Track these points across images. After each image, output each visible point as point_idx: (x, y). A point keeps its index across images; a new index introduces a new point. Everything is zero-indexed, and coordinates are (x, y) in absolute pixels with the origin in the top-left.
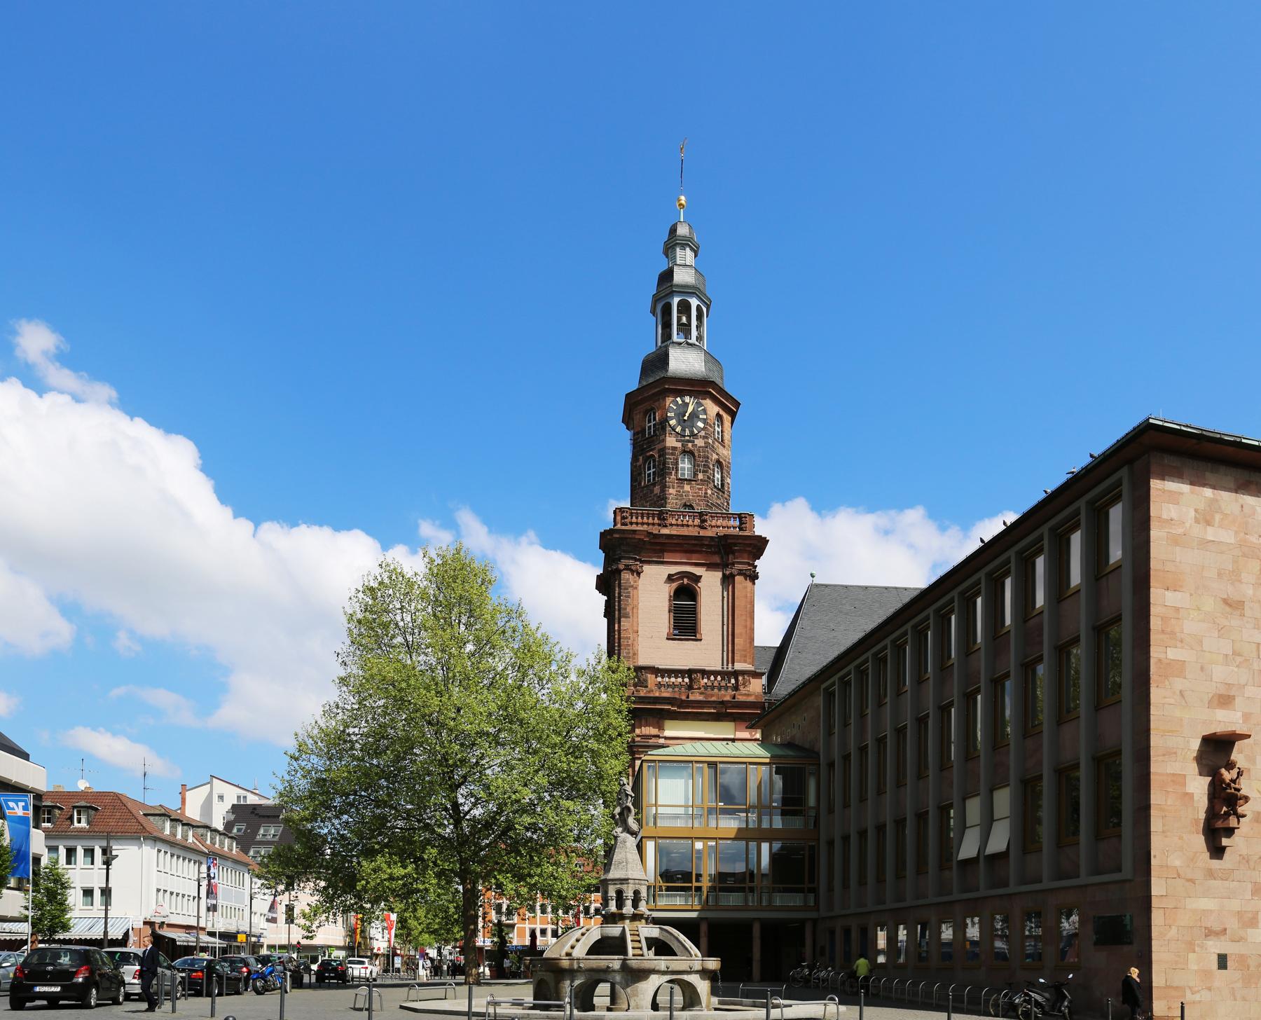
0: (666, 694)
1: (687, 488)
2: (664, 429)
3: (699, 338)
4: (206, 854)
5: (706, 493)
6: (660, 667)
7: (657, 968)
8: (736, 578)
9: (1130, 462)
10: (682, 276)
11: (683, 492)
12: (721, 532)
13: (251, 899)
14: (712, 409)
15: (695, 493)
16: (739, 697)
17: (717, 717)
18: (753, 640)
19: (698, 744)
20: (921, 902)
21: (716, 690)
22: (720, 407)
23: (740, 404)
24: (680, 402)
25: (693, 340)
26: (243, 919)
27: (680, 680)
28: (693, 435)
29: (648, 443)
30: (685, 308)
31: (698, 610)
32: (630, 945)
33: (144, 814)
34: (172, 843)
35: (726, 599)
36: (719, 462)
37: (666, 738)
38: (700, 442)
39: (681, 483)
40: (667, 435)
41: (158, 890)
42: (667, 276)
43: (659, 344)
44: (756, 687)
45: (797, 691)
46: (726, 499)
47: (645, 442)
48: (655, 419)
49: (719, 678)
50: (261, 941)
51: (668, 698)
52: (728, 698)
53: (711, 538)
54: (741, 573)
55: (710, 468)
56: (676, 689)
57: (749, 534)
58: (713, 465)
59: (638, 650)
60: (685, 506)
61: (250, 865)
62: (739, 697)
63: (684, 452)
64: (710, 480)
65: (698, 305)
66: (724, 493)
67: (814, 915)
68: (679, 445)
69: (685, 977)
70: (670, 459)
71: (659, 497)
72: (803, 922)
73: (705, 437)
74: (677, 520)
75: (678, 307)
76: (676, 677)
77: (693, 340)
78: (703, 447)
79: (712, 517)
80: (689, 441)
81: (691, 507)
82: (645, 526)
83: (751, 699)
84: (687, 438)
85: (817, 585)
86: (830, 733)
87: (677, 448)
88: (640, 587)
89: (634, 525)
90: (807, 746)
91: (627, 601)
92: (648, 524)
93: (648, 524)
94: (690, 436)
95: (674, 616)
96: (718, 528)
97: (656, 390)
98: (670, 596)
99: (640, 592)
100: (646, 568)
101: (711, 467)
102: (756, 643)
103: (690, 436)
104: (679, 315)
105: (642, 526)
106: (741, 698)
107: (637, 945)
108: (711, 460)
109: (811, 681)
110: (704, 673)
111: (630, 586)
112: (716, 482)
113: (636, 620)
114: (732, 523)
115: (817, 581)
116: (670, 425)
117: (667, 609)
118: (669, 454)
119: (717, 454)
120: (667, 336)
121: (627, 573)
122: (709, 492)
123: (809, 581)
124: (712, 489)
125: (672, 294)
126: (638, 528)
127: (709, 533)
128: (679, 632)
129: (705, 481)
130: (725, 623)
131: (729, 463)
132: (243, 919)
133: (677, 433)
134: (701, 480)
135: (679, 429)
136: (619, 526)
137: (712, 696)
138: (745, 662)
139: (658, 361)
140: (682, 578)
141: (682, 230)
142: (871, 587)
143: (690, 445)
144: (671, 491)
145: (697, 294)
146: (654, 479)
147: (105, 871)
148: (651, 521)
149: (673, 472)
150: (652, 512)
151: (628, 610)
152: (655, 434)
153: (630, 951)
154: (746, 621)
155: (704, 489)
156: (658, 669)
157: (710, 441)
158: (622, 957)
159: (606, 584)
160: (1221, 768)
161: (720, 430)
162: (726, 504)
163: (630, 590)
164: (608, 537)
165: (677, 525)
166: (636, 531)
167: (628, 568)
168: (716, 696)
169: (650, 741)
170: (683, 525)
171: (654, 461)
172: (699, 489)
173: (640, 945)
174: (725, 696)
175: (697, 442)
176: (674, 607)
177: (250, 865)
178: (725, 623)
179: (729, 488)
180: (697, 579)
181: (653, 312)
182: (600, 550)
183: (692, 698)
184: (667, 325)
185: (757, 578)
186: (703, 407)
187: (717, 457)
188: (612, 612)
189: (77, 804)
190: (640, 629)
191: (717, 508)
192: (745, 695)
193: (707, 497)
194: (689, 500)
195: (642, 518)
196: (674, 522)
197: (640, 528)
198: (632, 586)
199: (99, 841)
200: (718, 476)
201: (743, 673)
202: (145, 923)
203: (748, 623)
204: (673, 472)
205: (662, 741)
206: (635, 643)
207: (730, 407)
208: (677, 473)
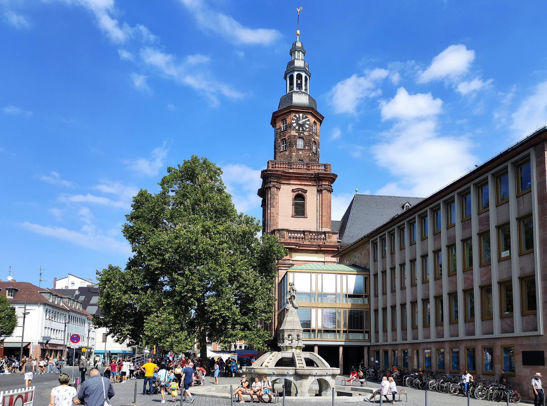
0: (293, 241)
1: (300, 153)
2: (290, 127)
3: (306, 90)
4: (68, 310)
5: (309, 155)
6: (290, 229)
7: (311, 374)
8: (323, 191)
9: (534, 146)
10: (299, 63)
12: (317, 172)
13: (89, 332)
14: (312, 119)
17: (316, 252)
19: (311, 264)
20: (428, 340)
21: (316, 240)
22: (315, 119)
23: (324, 118)
24: (298, 116)
25: (303, 90)
26: (83, 341)
27: (299, 235)
29: (283, 133)
30: (299, 77)
32: (297, 362)
33: (40, 293)
34: (53, 306)
35: (318, 200)
36: (314, 142)
37: (293, 261)
40: (292, 130)
41: (46, 328)
42: (292, 63)
44: (334, 239)
45: (358, 242)
46: (318, 157)
47: (282, 133)
48: (286, 123)
49: (314, 235)
50: (91, 351)
51: (295, 243)
52: (321, 244)
53: (312, 174)
54: (325, 189)
56: (298, 239)
57: (329, 173)
58: (312, 143)
61: (88, 316)
63: (300, 138)
64: (311, 149)
65: (305, 76)
66: (317, 155)
67: (369, 344)
68: (297, 134)
69: (323, 378)
72: (362, 347)
77: (303, 90)
79: (312, 165)
80: (302, 133)
85: (358, 195)
86: (375, 260)
87: (296, 135)
88: (279, 194)
89: (277, 168)
90: (363, 266)
92: (278, 167)
93: (278, 167)
96: (315, 170)
98: (293, 199)
99: (279, 197)
100: (282, 186)
102: (332, 219)
103: (302, 131)
104: (297, 80)
105: (281, 168)
106: (327, 244)
107: (301, 362)
109: (366, 237)
110: (310, 232)
111: (275, 194)
112: (313, 150)
114: (320, 168)
118: (292, 138)
119: (314, 139)
120: (291, 89)
122: (310, 154)
124: (312, 154)
125: (294, 71)
128: (296, 214)
130: (318, 210)
131: (319, 142)
132: (83, 341)
135: (297, 128)
136: (270, 168)
138: (327, 227)
139: (289, 97)
140: (298, 191)
141: (299, 44)
142: (383, 196)
143: (302, 134)
145: (305, 72)
146: (285, 149)
147: (23, 319)
148: (284, 166)
149: (294, 146)
150: (278, 162)
153: (298, 365)
154: (327, 210)
155: (308, 153)
156: (289, 230)
157: (311, 133)
158: (294, 368)
159: (263, 193)
161: (315, 128)
162: (317, 160)
164: (265, 173)
165: (296, 168)
166: (278, 170)
167: (274, 186)
168: (316, 242)
169: (286, 262)
170: (299, 169)
171: (286, 141)
173: (302, 362)
177: (88, 316)
178: (318, 210)
179: (319, 153)
180: (305, 191)
181: (285, 78)
182: (261, 179)
183: (305, 243)
184: (291, 84)
186: (308, 119)
188: (264, 204)
189: (8, 288)
195: (278, 165)
196: (295, 167)
197: (279, 169)
199: (18, 305)
200: (314, 148)
201: (329, 232)
202: (39, 343)
203: (329, 211)
204: (294, 146)
205: (291, 262)
206: (277, 218)
207: (320, 119)
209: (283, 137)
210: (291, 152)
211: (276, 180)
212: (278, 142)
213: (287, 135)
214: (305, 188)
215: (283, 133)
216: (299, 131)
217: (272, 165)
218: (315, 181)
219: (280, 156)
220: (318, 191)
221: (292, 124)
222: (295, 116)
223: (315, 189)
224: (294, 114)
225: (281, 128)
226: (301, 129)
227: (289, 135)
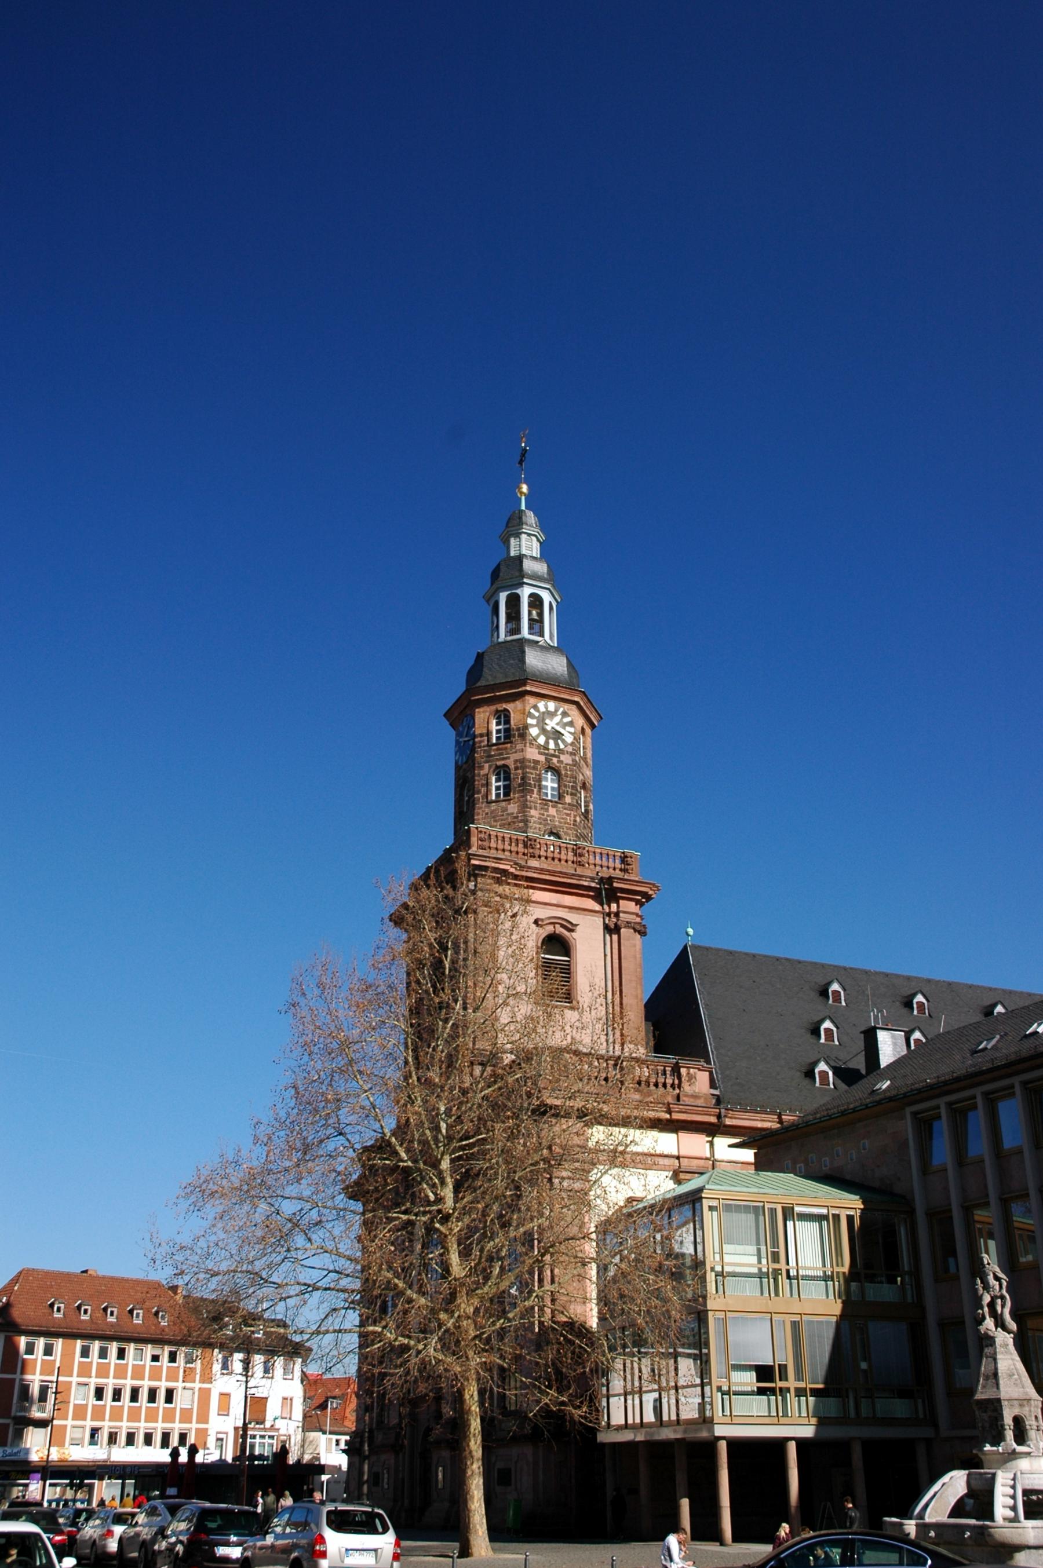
1: (552, 811)
5: (575, 821)
11: (548, 816)
16: (684, 1099)
26: (777, 1294)
29: (498, 749)
38: (566, 759)
40: (528, 745)
62: (684, 1099)
67: (928, 1432)
68: (542, 758)
70: (532, 776)
71: (517, 817)
73: (571, 754)
87: (539, 761)
98: (538, 948)
103: (555, 750)
118: (529, 767)
122: (578, 819)
129: (574, 805)
132: (777, 1294)
134: (569, 804)
143: (555, 760)
144: (533, 812)
157: (577, 759)
160: (979, 1331)
166: (501, 859)
172: (568, 815)
175: (562, 757)
180: (571, 928)
194: (555, 827)
208: (539, 791)
209: (498, 760)
210: (524, 807)
212: (482, 772)
213: (514, 757)
214: (573, 917)
215: (498, 749)
216: (548, 749)
218: (598, 898)
219: (487, 814)
220: (606, 928)
221: (526, 727)
222: (535, 707)
223: (598, 921)
225: (492, 733)
227: (518, 756)
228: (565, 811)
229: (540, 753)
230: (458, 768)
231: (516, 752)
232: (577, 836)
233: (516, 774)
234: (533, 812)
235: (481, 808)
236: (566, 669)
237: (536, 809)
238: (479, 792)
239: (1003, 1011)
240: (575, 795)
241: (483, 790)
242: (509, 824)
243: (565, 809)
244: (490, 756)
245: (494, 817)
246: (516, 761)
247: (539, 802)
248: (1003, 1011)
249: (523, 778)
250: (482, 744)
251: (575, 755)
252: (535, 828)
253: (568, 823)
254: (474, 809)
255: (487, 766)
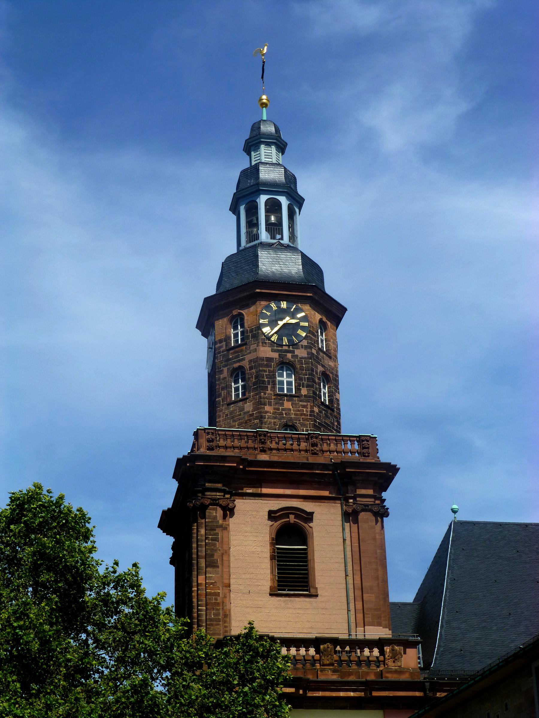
1: (287, 405)
5: (312, 411)
11: (283, 410)
12: (335, 458)
15: (299, 411)
18: (386, 595)
21: (354, 667)
28: (292, 344)
31: (310, 557)
35: (348, 542)
38: (301, 353)
39: (280, 399)
40: (260, 344)
43: (243, 243)
52: (372, 677)
55: (315, 383)
58: (319, 379)
59: (230, 610)
60: (286, 426)
64: (316, 396)
66: (333, 410)
68: (275, 355)
71: (252, 415)
73: (306, 347)
74: (277, 443)
75: (266, 206)
76: (298, 648)
77: (286, 240)
78: (305, 358)
81: (293, 427)
82: (236, 450)
83: (405, 677)
84: (286, 348)
91: (215, 545)
92: (241, 448)
94: (289, 346)
95: (278, 565)
97: (246, 294)
101: (317, 381)
103: (289, 346)
108: (317, 373)
113: (226, 570)
115: (461, 517)
116: (264, 334)
117: (268, 555)
118: (262, 365)
119: (323, 366)
121: (214, 509)
122: (316, 410)
123: (451, 517)
124: (319, 407)
126: (227, 454)
127: (321, 460)
129: (310, 397)
133: (273, 342)
136: (203, 451)
137: (350, 674)
143: (289, 355)
144: (267, 408)
146: (244, 394)
150: (231, 433)
151: (215, 557)
152: (244, 344)
155: (309, 407)
157: (314, 351)
162: (336, 424)
163: (218, 531)
170: (285, 450)
172: (304, 406)
174: (368, 673)
175: (297, 352)
176: (278, 553)
180: (309, 517)
185: (387, 516)
187: (322, 369)
190: (232, 582)
191: (327, 428)
192: (396, 672)
193: (314, 416)
196: (273, 445)
198: (221, 526)
203: (380, 573)
208: (274, 387)
209: (235, 362)
210: (259, 404)
211: (219, 486)
212: (222, 376)
213: (248, 357)
214: (308, 506)
217: (209, 441)
219: (227, 415)
221: (259, 327)
224: (264, 303)
226: (285, 341)
228: (301, 403)
229: (273, 351)
230: (209, 375)
231: (250, 353)
232: (315, 426)
233: (251, 374)
234: (267, 408)
235: (222, 410)
236: (301, 267)
237: (270, 404)
238: (220, 396)
239: (338, 647)
240: (312, 386)
241: (223, 393)
242: (246, 423)
243: (301, 401)
244: (228, 360)
245: (233, 418)
246: (250, 361)
247: (273, 397)
248: (338, 647)
249: (256, 377)
250: (221, 350)
251: (311, 348)
252: (270, 423)
253: (304, 415)
254: (216, 412)
255: (225, 369)
